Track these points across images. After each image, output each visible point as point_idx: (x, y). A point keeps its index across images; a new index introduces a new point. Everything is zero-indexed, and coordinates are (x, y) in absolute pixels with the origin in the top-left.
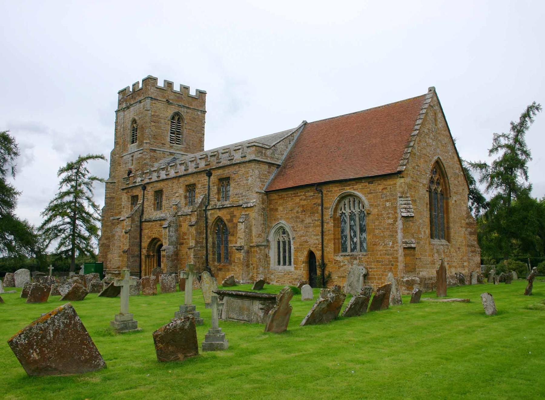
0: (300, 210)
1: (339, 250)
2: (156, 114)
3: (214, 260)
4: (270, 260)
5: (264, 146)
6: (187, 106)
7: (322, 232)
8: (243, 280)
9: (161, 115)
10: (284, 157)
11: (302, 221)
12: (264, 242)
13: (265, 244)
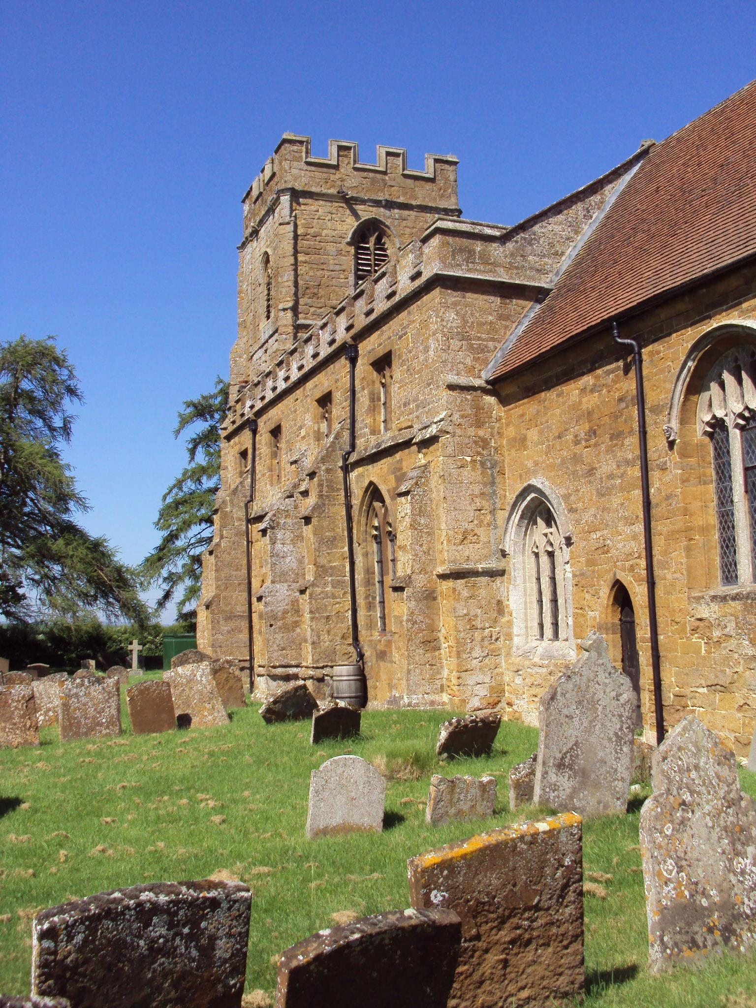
0: (582, 429)
1: (709, 575)
2: (311, 231)
3: (371, 626)
4: (510, 623)
5: (477, 229)
6: (401, 200)
7: (647, 504)
8: (410, 692)
9: (324, 233)
10: (565, 263)
11: (591, 471)
12: (487, 557)
13: (493, 564)
